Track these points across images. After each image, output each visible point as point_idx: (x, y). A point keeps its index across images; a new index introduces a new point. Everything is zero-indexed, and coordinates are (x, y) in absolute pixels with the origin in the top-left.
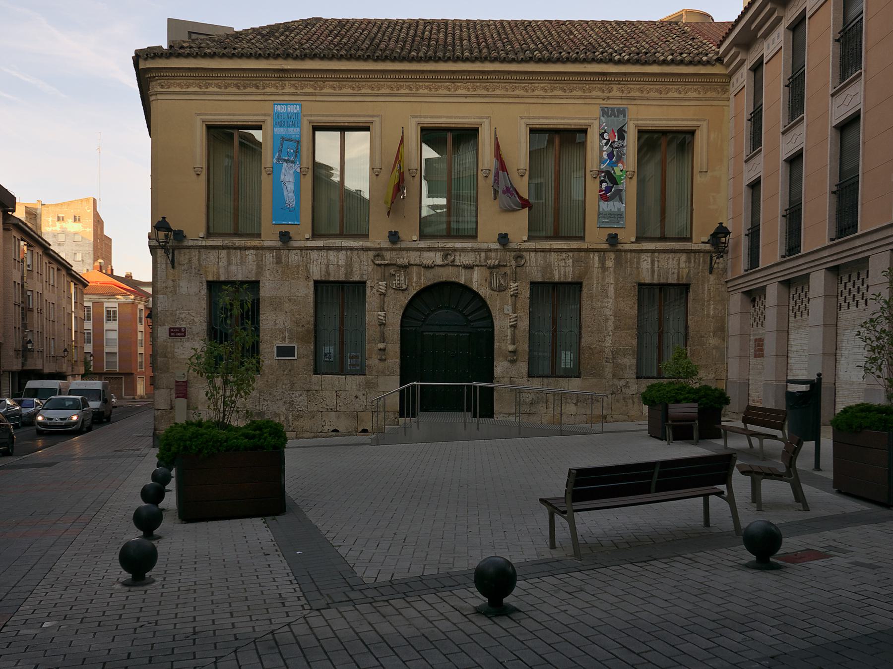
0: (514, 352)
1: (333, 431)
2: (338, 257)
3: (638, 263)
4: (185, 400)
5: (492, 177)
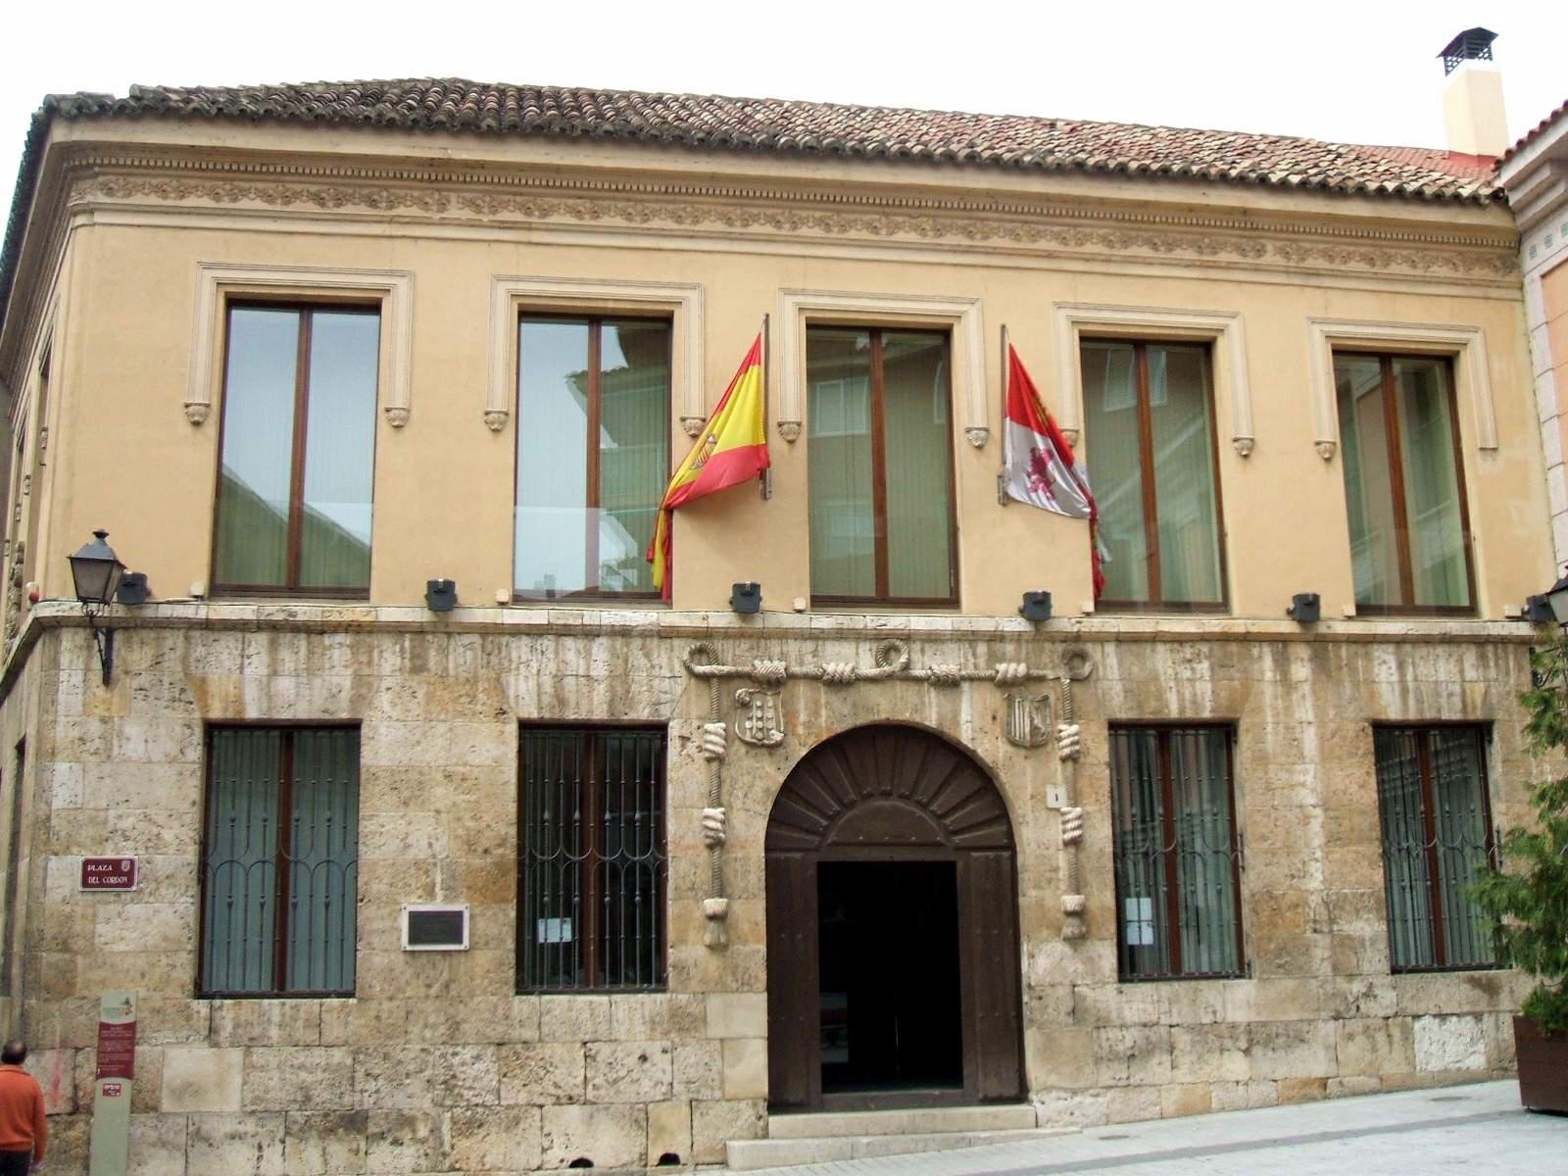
0: (1078, 914)
3: (1368, 670)
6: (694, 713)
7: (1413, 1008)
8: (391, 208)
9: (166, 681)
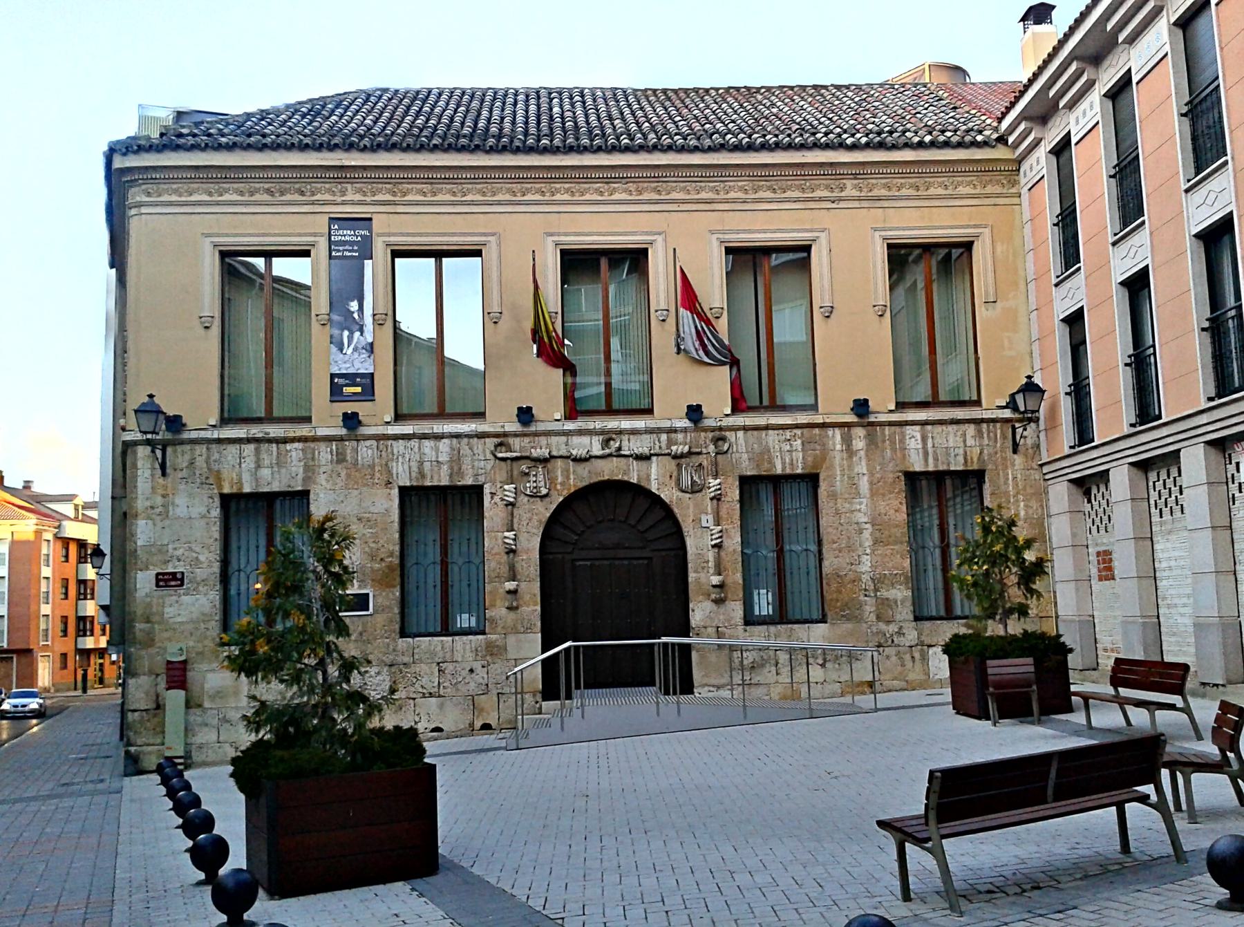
0: (721, 586)
1: (434, 730)
2: (437, 450)
3: (902, 441)
4: (183, 693)
5: (671, 320)
6: (498, 478)
7: (927, 641)
8: (313, 195)
9: (198, 473)
